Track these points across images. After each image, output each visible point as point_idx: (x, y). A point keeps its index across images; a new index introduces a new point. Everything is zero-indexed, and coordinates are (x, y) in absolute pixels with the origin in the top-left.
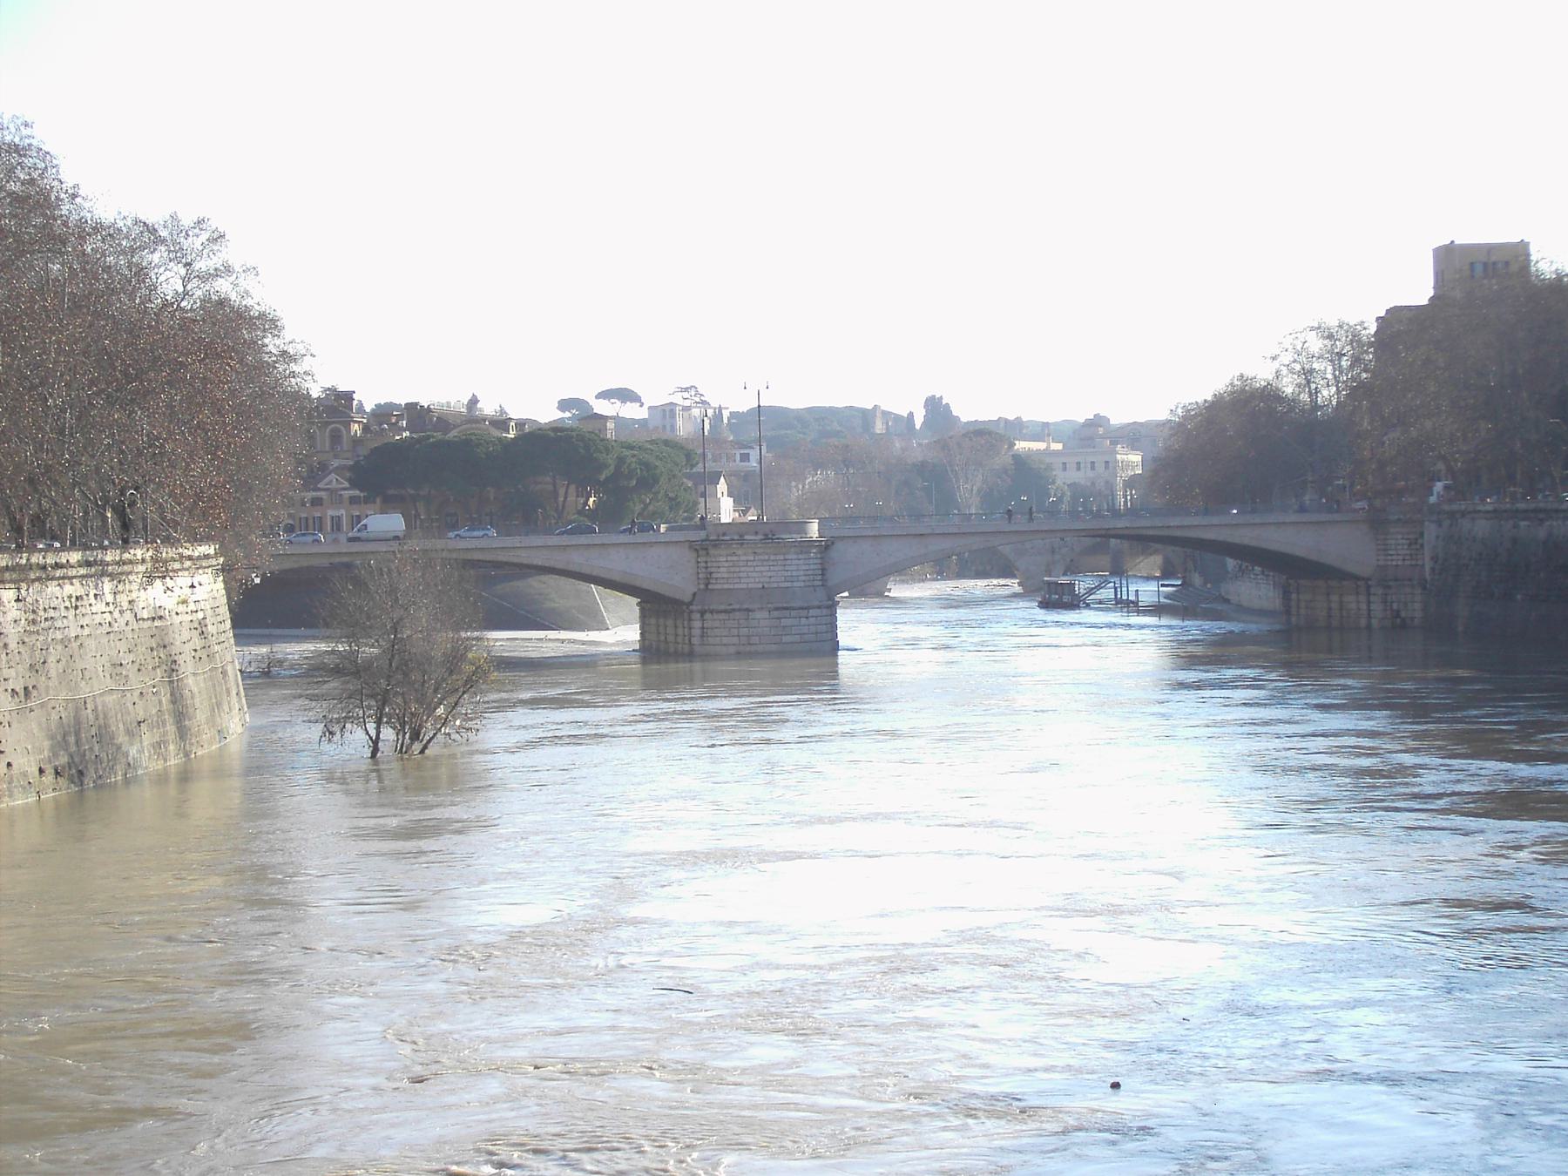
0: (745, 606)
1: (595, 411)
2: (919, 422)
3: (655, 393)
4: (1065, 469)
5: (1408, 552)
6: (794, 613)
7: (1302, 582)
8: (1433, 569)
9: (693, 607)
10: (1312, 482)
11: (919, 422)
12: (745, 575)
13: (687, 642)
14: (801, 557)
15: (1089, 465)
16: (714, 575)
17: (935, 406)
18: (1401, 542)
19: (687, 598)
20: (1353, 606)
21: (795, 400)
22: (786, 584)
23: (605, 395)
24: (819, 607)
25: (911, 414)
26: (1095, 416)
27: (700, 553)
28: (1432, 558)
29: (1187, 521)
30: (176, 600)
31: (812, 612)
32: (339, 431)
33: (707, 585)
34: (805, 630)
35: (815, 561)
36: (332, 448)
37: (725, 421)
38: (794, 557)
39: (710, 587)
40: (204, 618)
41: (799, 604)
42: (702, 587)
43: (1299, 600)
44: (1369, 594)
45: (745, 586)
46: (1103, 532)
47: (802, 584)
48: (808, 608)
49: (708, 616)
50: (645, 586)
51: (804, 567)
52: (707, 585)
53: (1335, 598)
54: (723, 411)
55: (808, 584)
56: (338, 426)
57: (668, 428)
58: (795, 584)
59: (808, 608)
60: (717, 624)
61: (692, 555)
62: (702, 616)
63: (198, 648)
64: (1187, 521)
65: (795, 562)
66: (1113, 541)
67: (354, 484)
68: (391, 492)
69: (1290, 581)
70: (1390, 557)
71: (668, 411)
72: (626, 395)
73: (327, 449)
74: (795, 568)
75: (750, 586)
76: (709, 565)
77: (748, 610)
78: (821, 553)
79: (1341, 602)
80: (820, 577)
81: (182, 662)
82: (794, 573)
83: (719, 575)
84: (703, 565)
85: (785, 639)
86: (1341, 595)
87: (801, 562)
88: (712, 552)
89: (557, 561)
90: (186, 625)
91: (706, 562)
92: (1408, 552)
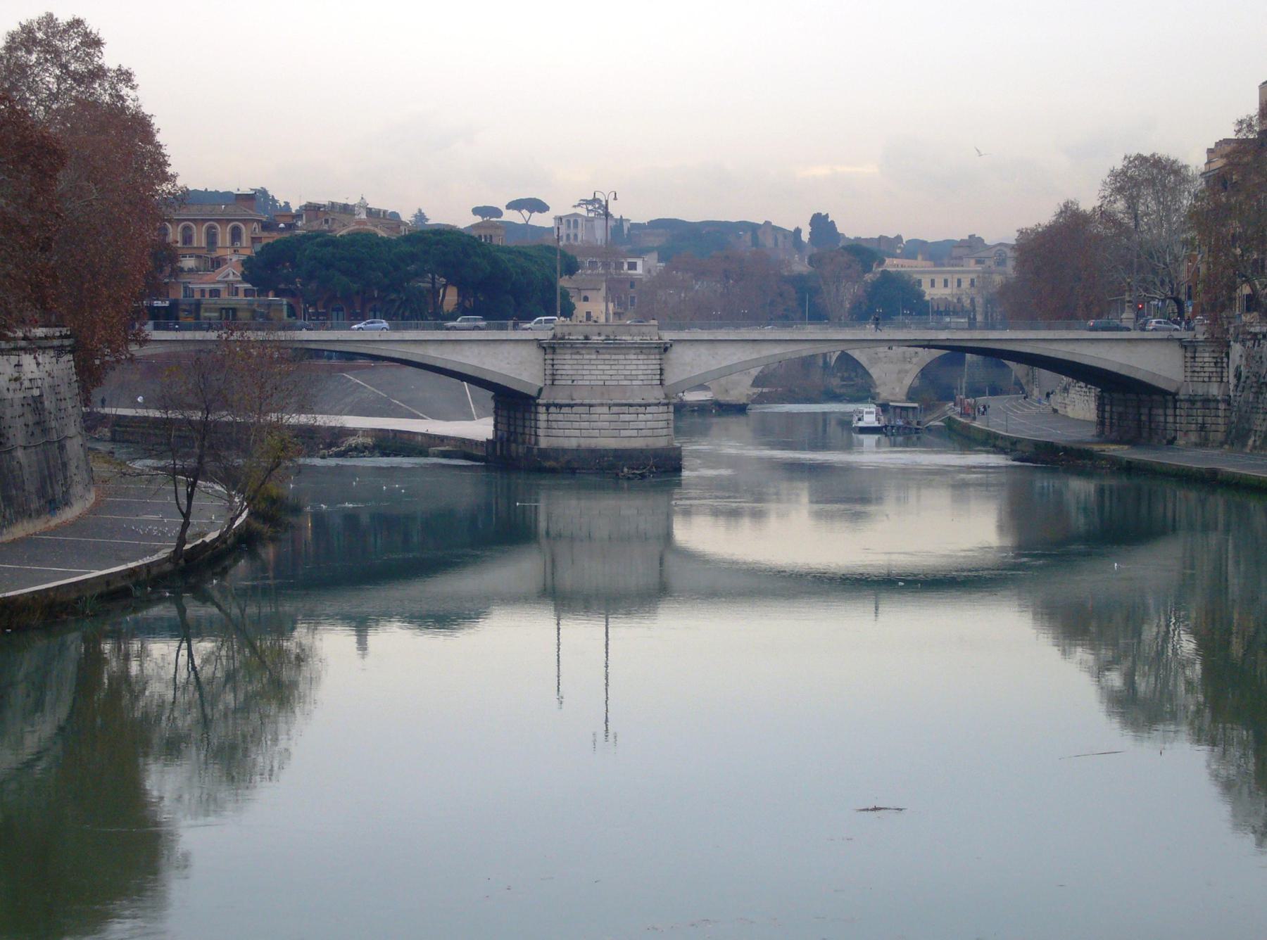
0: (587, 401)
1: (1195, 159)
2: (805, 237)
3: (562, 204)
4: (933, 284)
5: (1214, 369)
6: (632, 410)
7: (1115, 395)
8: (1237, 386)
9: (540, 401)
10: (1129, 302)
11: (805, 237)
12: (587, 372)
13: (533, 433)
14: (640, 357)
15: (949, 284)
16: (559, 372)
17: (821, 223)
18: (1206, 360)
19: (534, 393)
20: (1162, 419)
21: (653, 219)
22: (625, 383)
23: (516, 205)
24: (657, 405)
25: (798, 231)
26: (970, 237)
27: (548, 351)
28: (1235, 376)
29: (1008, 334)
30: (7, 379)
31: (649, 409)
32: (214, 228)
33: (553, 380)
34: (642, 425)
35: (654, 362)
36: (233, 244)
37: (626, 231)
38: (635, 357)
39: (556, 383)
40: (41, 396)
41: (639, 401)
42: (549, 382)
43: (1111, 412)
44: (1175, 408)
45: (588, 383)
46: (926, 343)
47: (640, 383)
48: (646, 405)
49: (552, 409)
50: (495, 380)
51: (643, 367)
52: (553, 380)
53: (1144, 411)
54: (624, 223)
55: (645, 382)
56: (212, 223)
57: (572, 236)
58: (635, 383)
59: (646, 405)
60: (560, 417)
61: (1180, 352)
62: (547, 410)
63: (30, 423)
64: (1008, 334)
65: (634, 362)
66: (968, 356)
67: (245, 279)
68: (282, 286)
69: (1104, 394)
70: (1196, 374)
71: (572, 221)
72: (537, 206)
73: (228, 244)
74: (635, 367)
75: (592, 383)
76: (555, 362)
77: (591, 406)
78: (660, 354)
79: (1150, 415)
80: (557, 377)
81: (11, 436)
82: (634, 372)
83: (563, 372)
84: (551, 362)
85: (624, 433)
86: (1150, 409)
87: (641, 362)
88: (558, 351)
89: (415, 353)
90: (17, 403)
91: (553, 360)
92: (1214, 369)
